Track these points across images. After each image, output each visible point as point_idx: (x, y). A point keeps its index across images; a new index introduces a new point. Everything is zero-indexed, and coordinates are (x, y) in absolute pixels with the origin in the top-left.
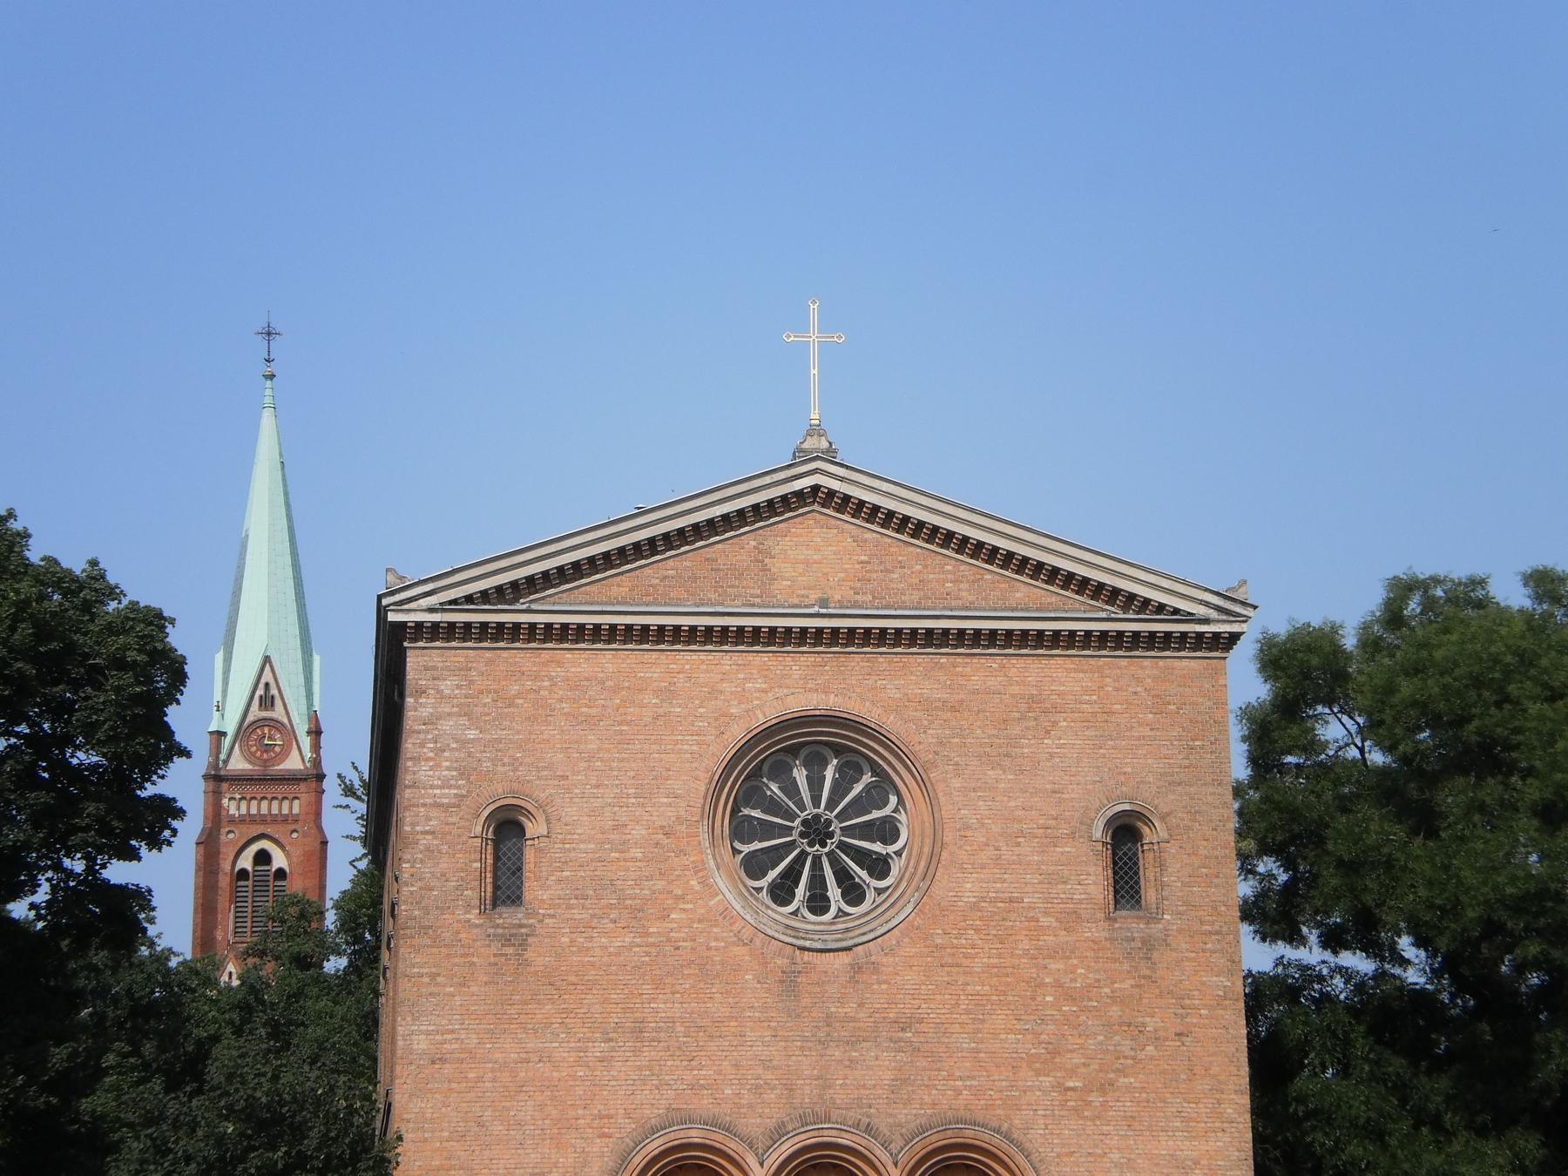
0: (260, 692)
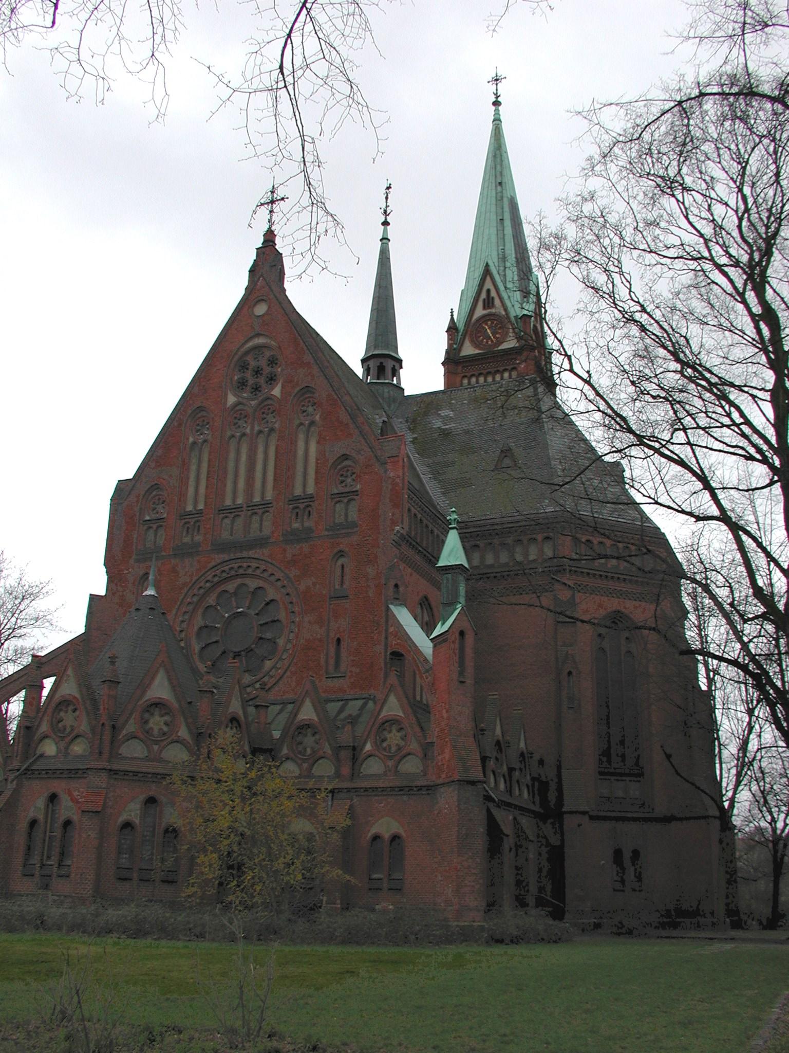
0: (484, 295)
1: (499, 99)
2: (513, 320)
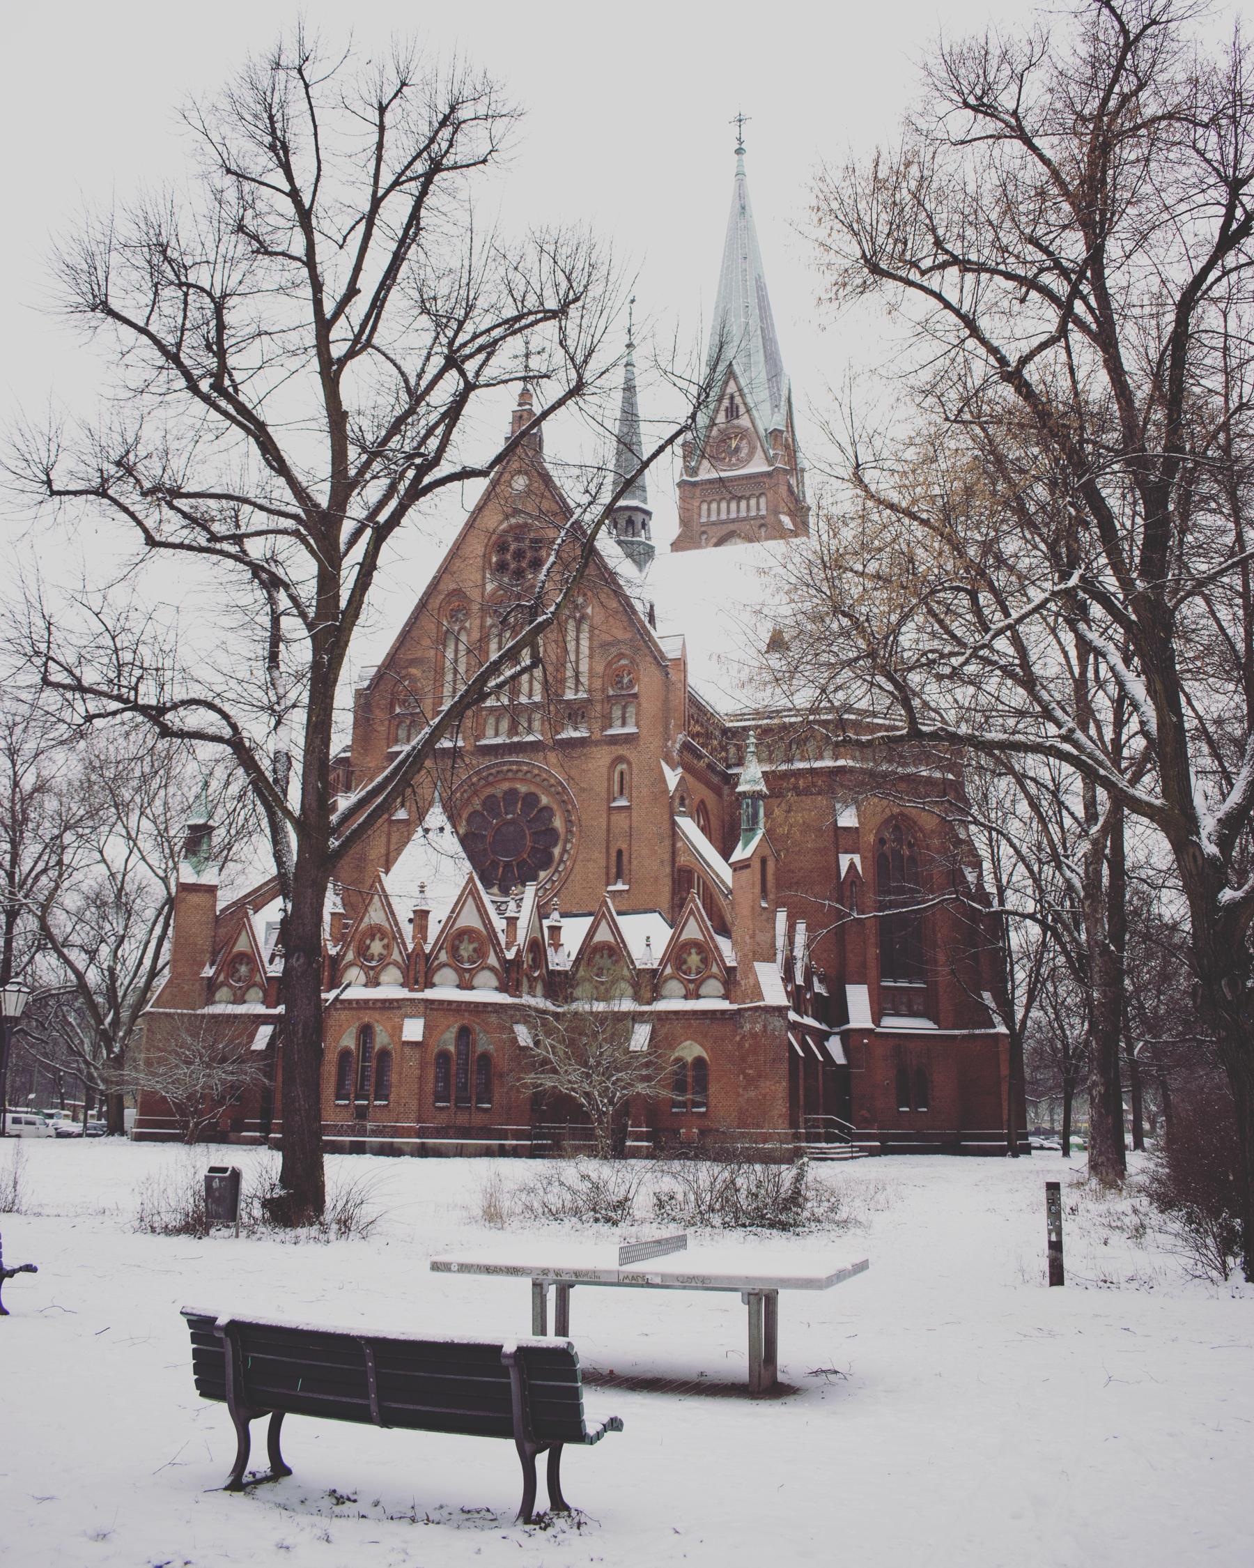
0: (726, 403)
1: (743, 146)
2: (762, 433)
